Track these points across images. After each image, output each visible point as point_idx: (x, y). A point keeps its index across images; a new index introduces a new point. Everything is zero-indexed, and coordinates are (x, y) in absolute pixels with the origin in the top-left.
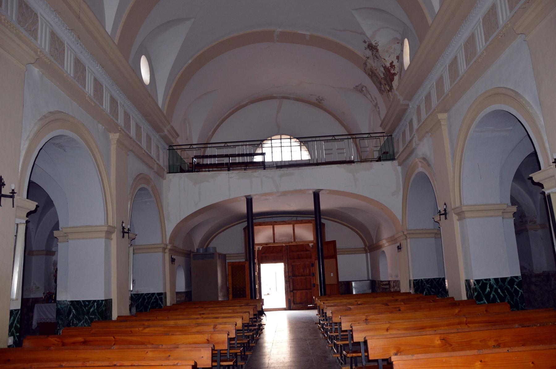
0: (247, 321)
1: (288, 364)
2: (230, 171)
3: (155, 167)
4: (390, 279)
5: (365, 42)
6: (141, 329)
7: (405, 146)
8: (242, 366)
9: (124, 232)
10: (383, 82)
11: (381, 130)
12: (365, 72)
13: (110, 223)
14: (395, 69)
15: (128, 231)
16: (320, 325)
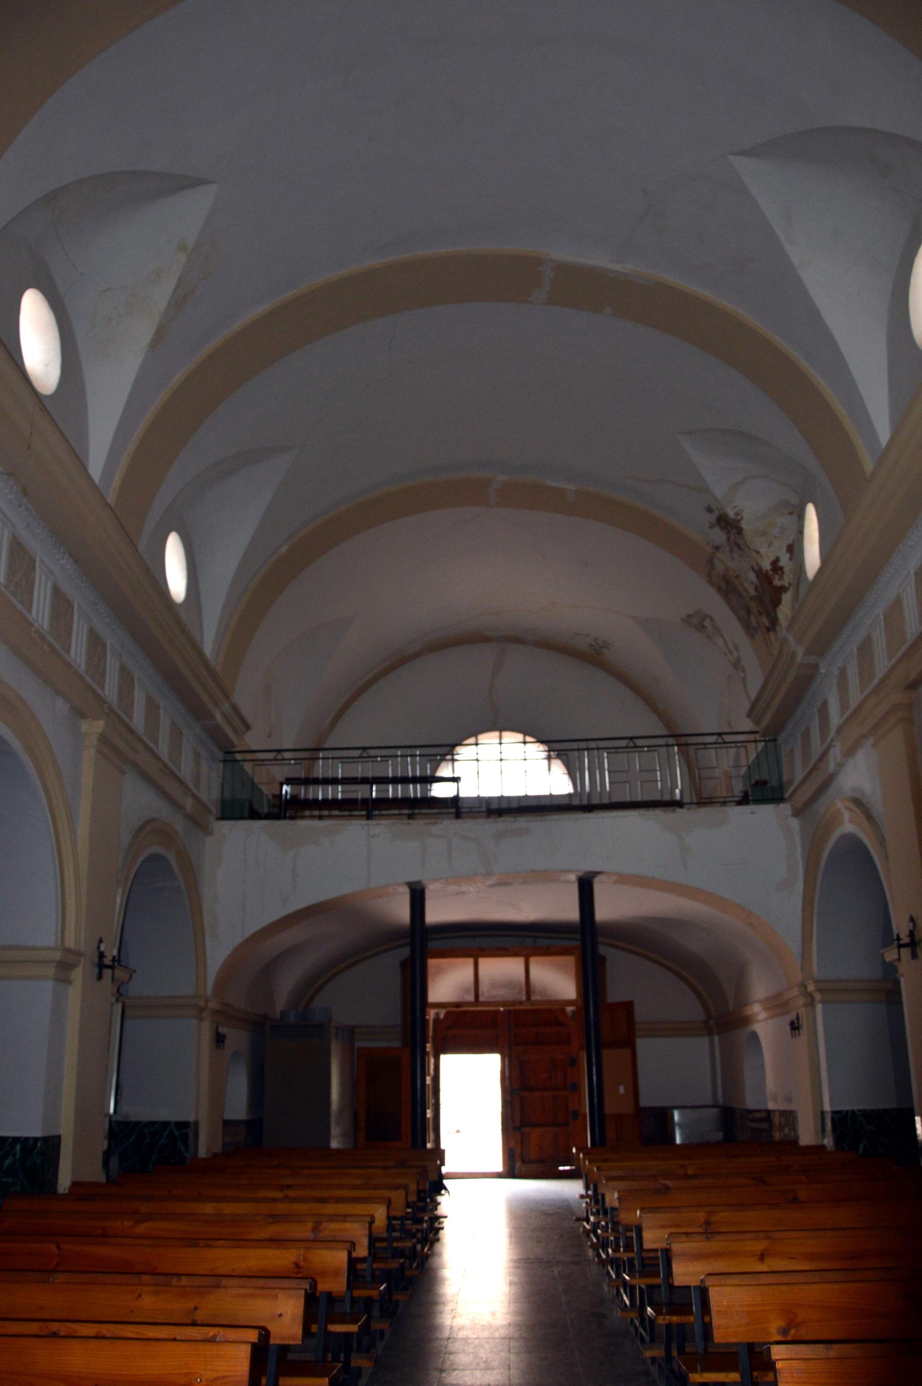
0: (400, 1209)
1: (503, 1332)
2: (371, 819)
3: (189, 803)
4: (771, 1106)
5: (709, 510)
6: (127, 1224)
7: (811, 766)
8: (382, 1333)
9: (101, 966)
10: (753, 605)
11: (748, 725)
12: (711, 583)
13: (70, 943)
14: (785, 577)
15: (110, 963)
16: (588, 1223)
